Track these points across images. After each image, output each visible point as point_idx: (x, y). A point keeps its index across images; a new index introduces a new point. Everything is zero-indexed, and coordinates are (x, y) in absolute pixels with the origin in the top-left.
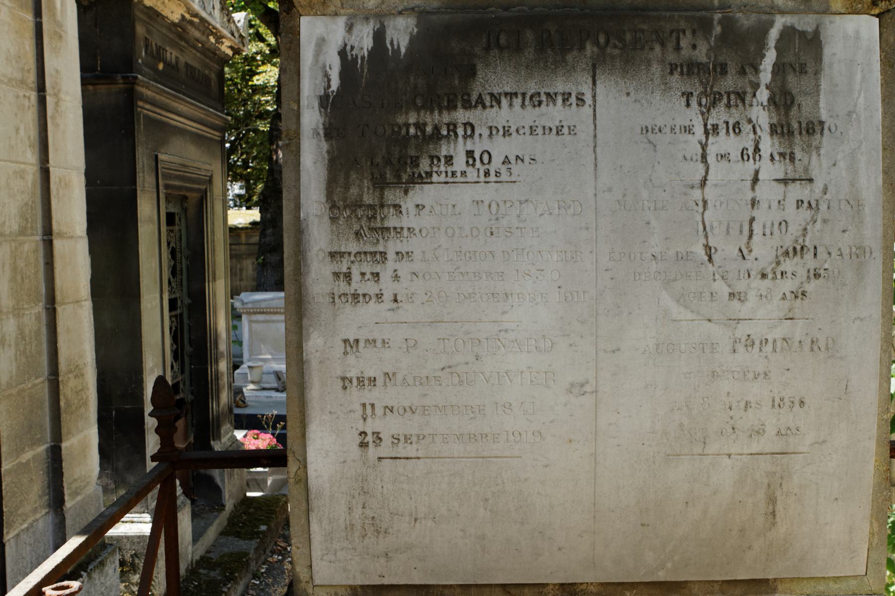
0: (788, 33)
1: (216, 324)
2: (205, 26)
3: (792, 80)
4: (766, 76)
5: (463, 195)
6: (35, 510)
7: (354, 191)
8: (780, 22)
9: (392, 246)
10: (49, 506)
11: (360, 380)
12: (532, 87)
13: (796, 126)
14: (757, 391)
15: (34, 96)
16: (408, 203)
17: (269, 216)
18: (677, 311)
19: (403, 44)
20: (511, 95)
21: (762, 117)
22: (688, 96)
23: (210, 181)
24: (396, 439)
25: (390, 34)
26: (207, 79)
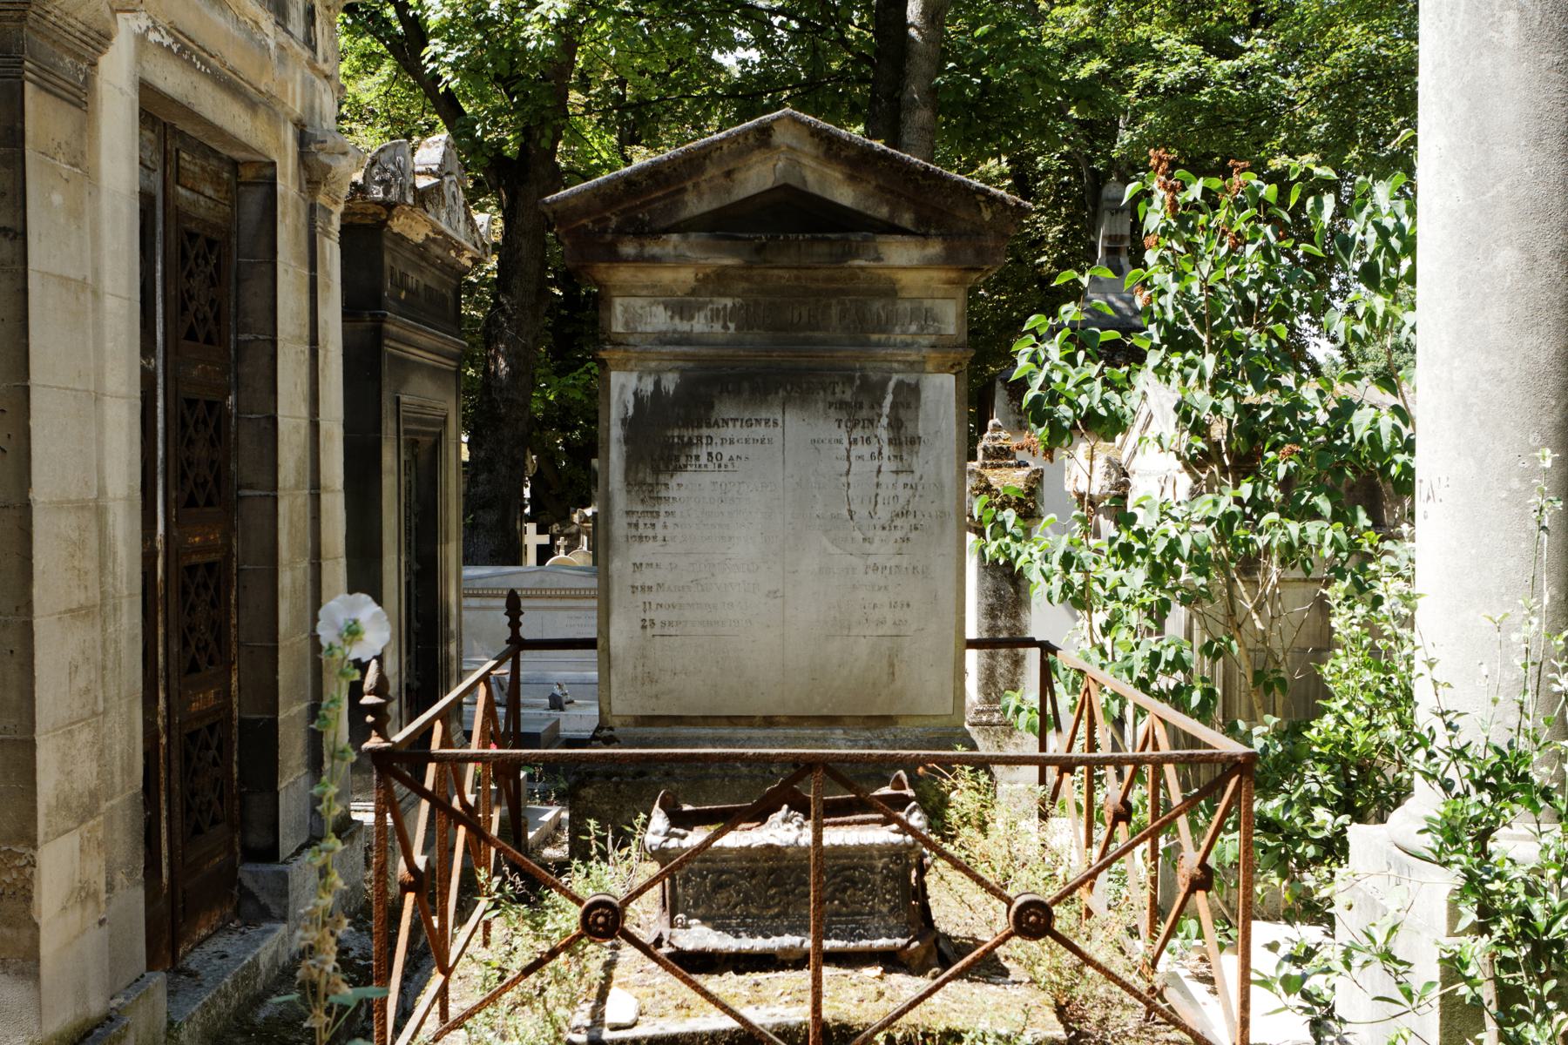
0: (900, 384)
1: (447, 596)
2: (449, 243)
3: (902, 413)
4: (886, 409)
5: (705, 478)
6: (298, 767)
7: (641, 475)
8: (895, 378)
9: (663, 508)
10: (308, 766)
11: (643, 588)
12: (747, 415)
13: (904, 439)
14: (881, 598)
15: (306, 348)
16: (673, 483)
17: (482, 454)
18: (832, 549)
19: (672, 389)
20: (735, 420)
21: (884, 434)
22: (839, 421)
23: (445, 422)
24: (663, 623)
25: (664, 383)
26: (444, 297)
